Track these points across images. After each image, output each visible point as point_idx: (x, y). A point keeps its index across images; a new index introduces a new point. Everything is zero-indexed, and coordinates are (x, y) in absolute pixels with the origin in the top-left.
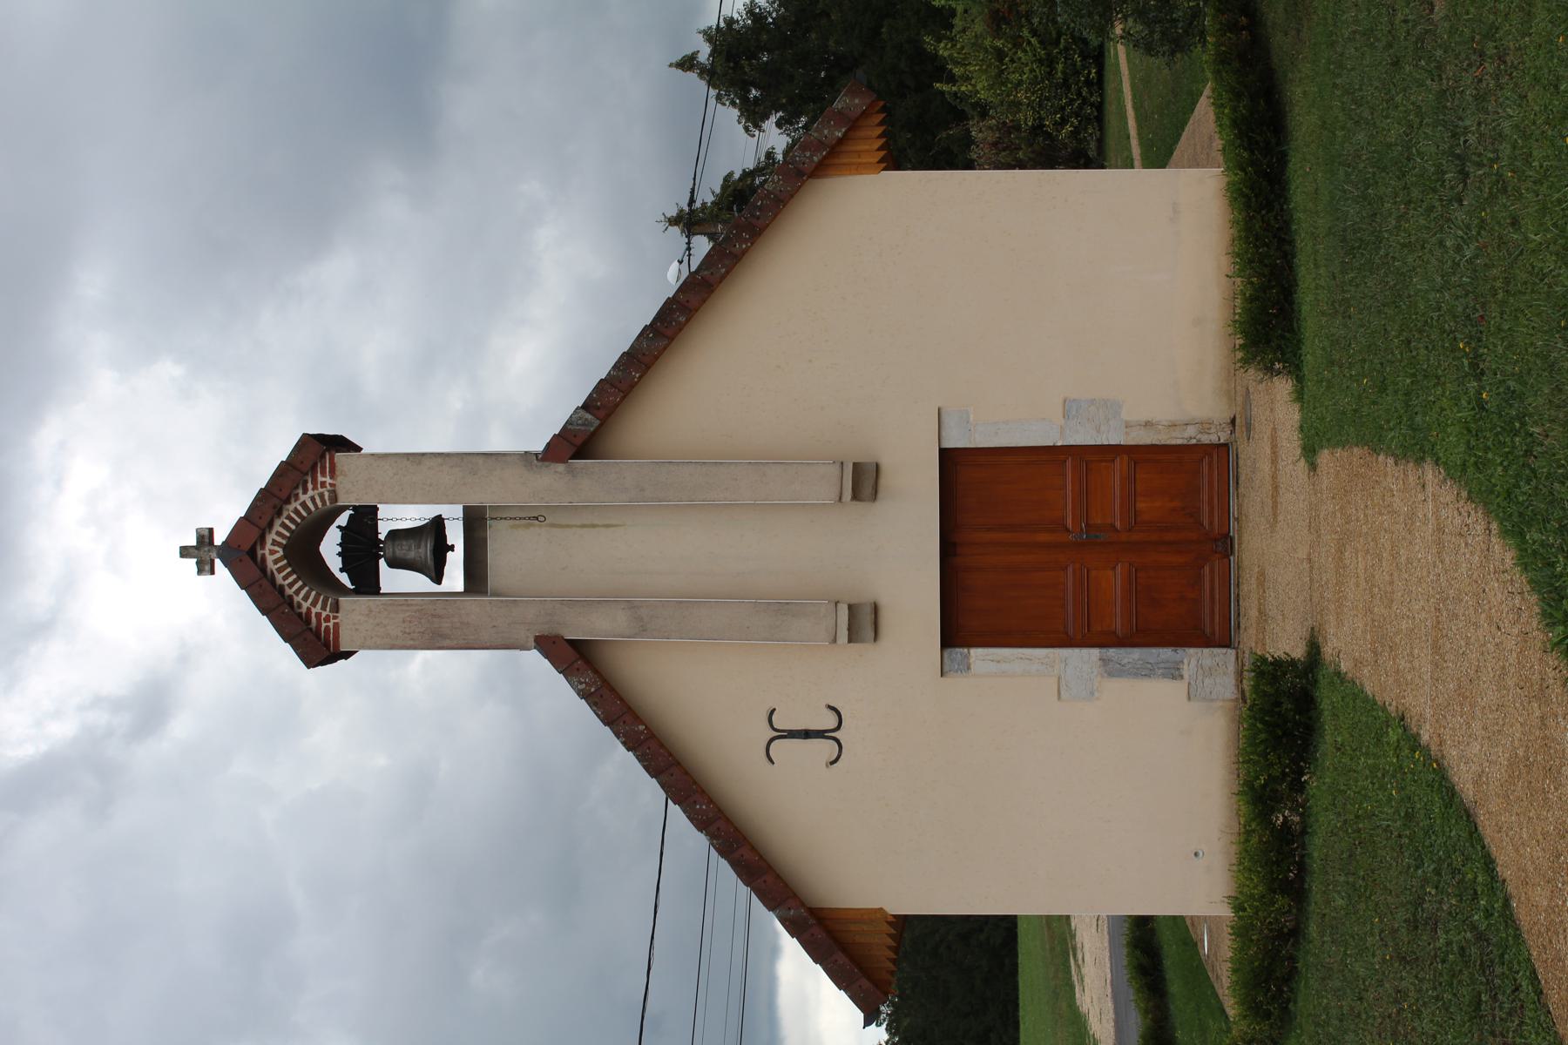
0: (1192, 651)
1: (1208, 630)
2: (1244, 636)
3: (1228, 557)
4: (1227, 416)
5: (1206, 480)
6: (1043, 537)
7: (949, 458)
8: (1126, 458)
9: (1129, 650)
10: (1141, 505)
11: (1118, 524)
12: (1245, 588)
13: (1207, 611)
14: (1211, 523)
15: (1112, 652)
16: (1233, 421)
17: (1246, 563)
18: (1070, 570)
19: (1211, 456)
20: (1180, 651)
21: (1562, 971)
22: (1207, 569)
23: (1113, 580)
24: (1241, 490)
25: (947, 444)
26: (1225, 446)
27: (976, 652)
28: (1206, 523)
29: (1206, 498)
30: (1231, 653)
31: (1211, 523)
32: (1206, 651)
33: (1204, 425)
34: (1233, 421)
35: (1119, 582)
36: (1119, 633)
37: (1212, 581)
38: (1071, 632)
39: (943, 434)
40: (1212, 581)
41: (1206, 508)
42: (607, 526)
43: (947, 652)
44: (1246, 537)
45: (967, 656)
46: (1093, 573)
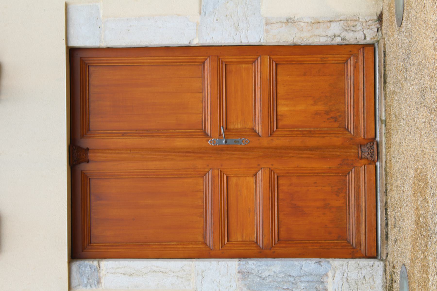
0: (337, 263)
1: (353, 241)
2: (392, 248)
3: (374, 162)
4: (374, 12)
5: (351, 82)
6: (181, 143)
7: (78, 60)
8: (266, 59)
9: (270, 261)
10: (283, 109)
11: (259, 129)
12: (394, 196)
13: (353, 220)
14: (356, 128)
15: (252, 264)
16: (380, 18)
17: (396, 167)
18: (209, 176)
19: (356, 57)
20: (324, 261)
21: (435, 89)
22: (352, 175)
23: (252, 189)
24: (391, 87)
25: (75, 43)
26: (371, 47)
27: (108, 266)
28: (351, 127)
29: (351, 101)
30: (378, 265)
31: (356, 128)
32: (352, 262)
33: (350, 22)
34: (380, 18)
35: (260, 189)
36: (260, 243)
37: (358, 188)
38: (210, 242)
39: (72, 31)
40: (358, 188)
41: (351, 112)
42: (385, 55)
43: (76, 265)
44: (395, 139)
45: (98, 269)
46: (233, 181)
